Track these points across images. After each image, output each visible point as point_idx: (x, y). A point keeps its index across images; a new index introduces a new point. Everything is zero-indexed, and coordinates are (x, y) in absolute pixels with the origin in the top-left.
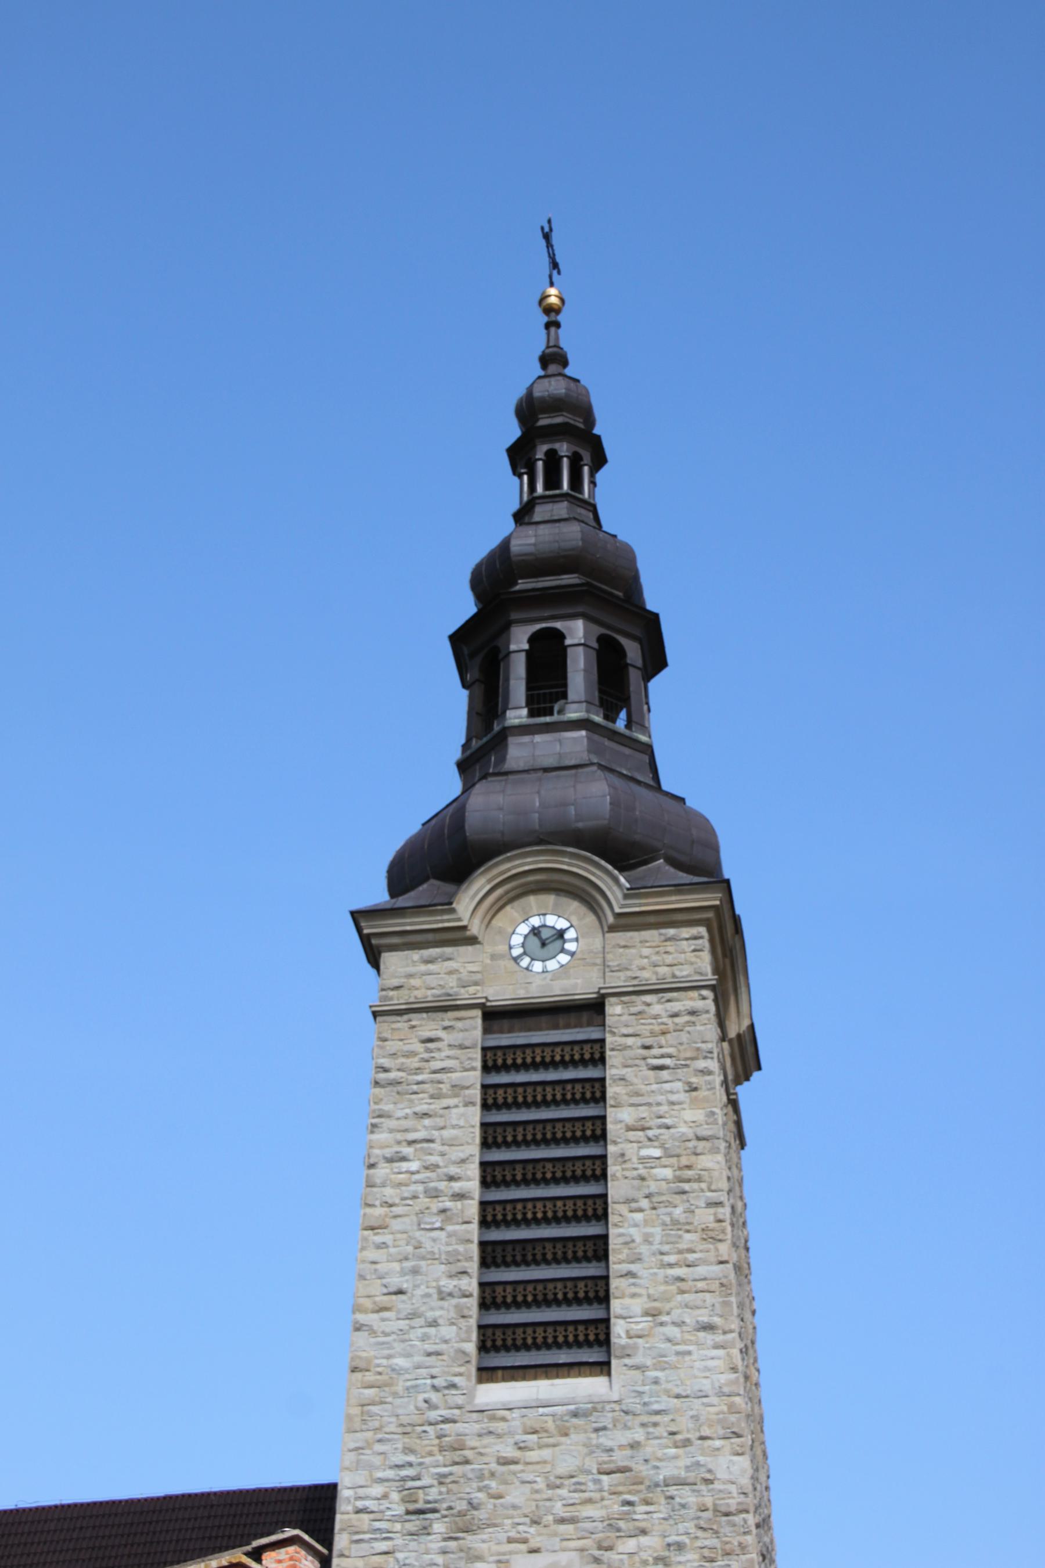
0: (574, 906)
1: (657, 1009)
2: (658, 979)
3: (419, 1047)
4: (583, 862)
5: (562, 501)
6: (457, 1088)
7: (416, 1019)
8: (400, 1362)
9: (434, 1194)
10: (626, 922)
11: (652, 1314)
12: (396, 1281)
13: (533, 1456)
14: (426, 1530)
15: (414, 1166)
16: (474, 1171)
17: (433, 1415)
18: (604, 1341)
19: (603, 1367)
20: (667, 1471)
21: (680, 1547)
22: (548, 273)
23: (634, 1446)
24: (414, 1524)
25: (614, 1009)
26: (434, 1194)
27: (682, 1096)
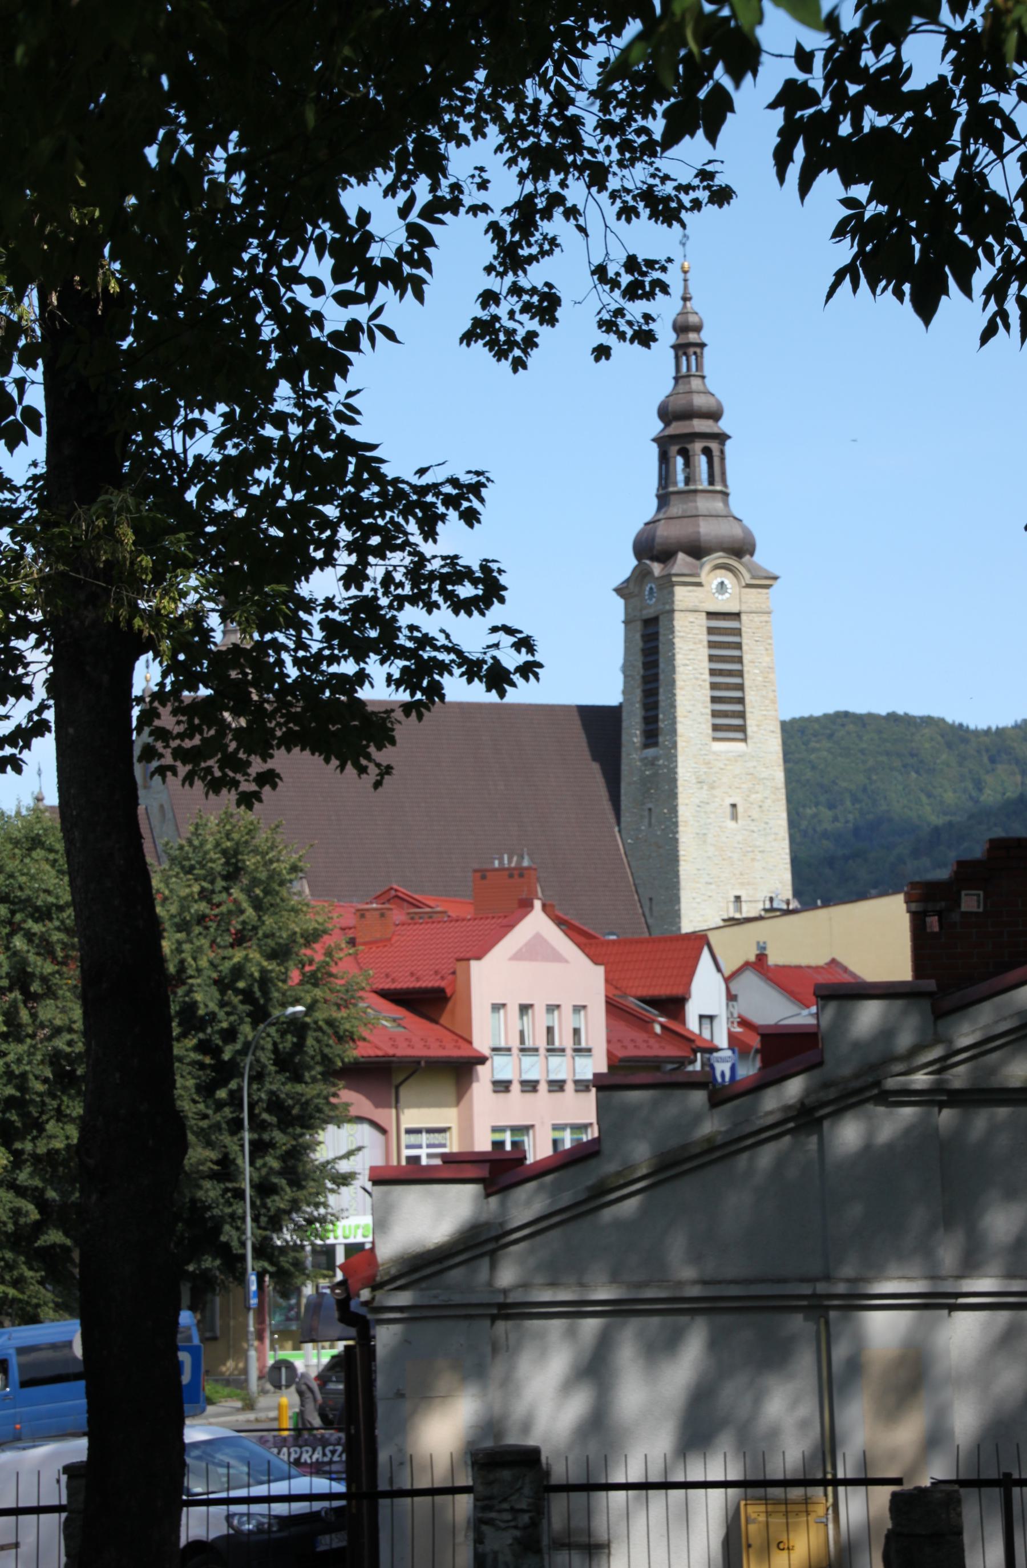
0: (730, 575)
1: (756, 619)
2: (753, 577)
3: (687, 624)
4: (650, 1304)
5: (856, 1076)
6: (701, 641)
7: (688, 614)
8: (692, 735)
9: (697, 679)
10: (749, 586)
11: (758, 726)
12: (690, 708)
13: (729, 767)
14: (702, 788)
15: (690, 668)
16: (707, 672)
17: (703, 752)
18: (742, 729)
19: (745, 740)
20: (763, 775)
21: (766, 798)
22: (746, 522)
23: (755, 767)
24: (699, 785)
25: (744, 617)
26: (697, 679)
27: (764, 652)
